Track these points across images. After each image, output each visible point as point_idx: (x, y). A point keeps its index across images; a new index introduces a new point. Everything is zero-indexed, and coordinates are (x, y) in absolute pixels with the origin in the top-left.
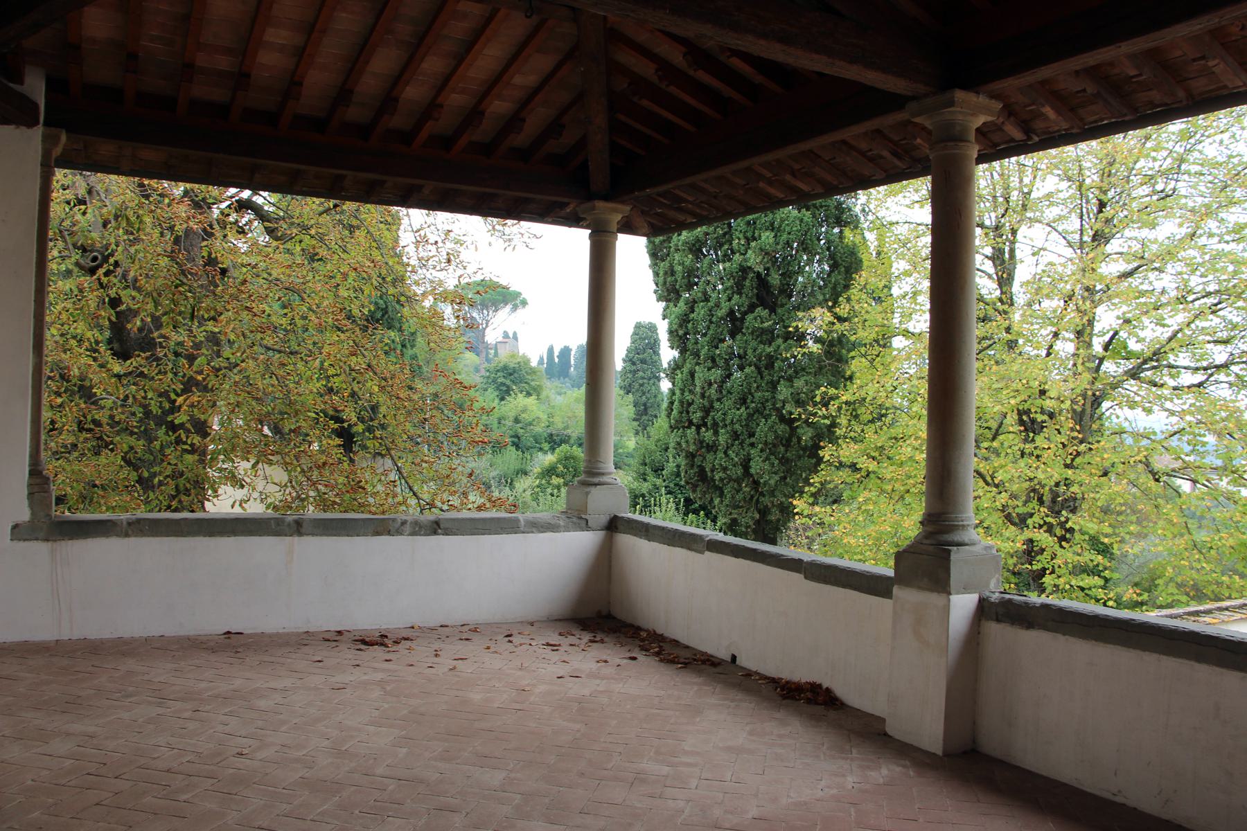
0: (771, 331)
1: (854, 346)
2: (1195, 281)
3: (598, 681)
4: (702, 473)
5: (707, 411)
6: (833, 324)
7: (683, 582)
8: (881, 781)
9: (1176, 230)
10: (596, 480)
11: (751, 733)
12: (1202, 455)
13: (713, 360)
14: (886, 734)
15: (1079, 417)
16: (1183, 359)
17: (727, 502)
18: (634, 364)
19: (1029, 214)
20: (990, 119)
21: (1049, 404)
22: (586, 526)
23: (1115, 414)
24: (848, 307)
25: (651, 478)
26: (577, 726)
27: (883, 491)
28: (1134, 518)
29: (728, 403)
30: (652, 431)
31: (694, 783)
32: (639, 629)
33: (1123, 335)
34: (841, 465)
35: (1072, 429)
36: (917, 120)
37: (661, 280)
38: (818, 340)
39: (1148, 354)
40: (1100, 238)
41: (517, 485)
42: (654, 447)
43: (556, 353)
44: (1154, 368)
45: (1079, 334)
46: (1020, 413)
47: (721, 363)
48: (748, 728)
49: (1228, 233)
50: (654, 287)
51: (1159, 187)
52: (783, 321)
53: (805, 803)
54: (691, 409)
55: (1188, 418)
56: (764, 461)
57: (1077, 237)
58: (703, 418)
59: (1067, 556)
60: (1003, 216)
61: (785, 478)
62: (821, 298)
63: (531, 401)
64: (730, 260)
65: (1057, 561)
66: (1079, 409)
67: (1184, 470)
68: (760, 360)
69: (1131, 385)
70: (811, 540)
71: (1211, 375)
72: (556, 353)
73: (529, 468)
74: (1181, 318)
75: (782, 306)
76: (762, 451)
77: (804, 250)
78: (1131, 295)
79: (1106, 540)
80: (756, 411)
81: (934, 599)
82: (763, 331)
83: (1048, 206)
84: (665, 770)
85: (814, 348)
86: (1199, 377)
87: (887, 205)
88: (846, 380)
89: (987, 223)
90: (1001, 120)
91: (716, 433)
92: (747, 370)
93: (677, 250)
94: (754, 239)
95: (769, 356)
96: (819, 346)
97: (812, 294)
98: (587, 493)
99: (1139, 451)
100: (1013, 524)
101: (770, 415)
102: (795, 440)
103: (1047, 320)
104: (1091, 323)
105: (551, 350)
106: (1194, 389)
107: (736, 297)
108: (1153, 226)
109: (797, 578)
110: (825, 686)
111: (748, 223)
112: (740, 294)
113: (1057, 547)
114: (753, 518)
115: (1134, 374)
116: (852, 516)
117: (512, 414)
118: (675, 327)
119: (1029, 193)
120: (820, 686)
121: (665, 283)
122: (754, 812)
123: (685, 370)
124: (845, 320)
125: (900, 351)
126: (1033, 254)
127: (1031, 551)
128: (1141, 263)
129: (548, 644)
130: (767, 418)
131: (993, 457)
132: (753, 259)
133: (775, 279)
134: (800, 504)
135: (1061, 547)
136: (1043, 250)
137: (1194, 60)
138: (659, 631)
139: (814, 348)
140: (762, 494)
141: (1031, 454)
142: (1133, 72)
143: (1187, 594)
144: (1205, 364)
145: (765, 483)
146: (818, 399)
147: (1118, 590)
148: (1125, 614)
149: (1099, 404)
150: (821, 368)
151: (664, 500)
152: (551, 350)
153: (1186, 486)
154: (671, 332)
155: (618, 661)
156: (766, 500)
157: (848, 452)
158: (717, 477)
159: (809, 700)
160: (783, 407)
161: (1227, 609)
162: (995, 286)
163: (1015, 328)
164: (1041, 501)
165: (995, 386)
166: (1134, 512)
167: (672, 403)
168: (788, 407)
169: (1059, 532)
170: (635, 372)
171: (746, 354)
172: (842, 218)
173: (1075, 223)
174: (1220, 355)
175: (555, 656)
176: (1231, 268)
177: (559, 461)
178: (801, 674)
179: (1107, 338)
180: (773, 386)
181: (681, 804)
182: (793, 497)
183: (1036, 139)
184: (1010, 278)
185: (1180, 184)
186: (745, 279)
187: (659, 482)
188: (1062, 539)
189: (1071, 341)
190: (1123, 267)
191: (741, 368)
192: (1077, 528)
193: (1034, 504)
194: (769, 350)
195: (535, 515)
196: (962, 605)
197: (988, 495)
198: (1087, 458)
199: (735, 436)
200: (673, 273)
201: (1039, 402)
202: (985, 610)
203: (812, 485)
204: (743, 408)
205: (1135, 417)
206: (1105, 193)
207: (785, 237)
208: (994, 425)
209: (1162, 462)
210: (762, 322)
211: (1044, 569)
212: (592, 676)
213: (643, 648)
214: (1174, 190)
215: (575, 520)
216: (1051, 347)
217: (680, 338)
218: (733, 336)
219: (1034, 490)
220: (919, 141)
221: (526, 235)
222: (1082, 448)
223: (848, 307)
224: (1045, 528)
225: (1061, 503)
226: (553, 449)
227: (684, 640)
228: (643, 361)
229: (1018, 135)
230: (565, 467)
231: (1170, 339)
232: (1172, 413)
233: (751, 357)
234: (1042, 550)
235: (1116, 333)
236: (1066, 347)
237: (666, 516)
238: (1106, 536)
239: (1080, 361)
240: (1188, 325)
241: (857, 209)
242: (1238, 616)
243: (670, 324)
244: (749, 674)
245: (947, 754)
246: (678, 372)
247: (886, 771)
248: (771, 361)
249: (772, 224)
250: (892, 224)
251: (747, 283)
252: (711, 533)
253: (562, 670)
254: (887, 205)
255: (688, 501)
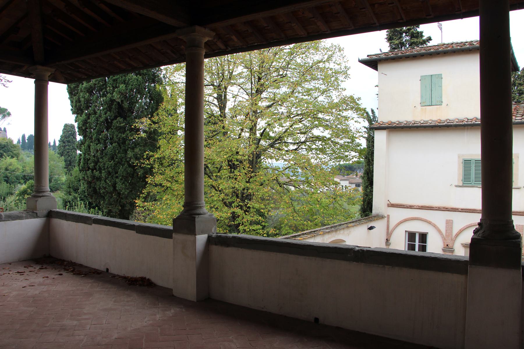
0: (124, 127)
1: (161, 134)
2: (293, 109)
3: (43, 287)
4: (95, 191)
5: (96, 163)
6: (151, 125)
7: (87, 239)
8: (171, 315)
9: (287, 90)
10: (41, 195)
11: (115, 302)
12: (297, 176)
13: (99, 140)
14: (173, 296)
15: (251, 163)
16: (290, 140)
17: (106, 202)
18: (64, 143)
19: (232, 81)
20: (210, 39)
21: (239, 157)
22: (36, 216)
23: (268, 162)
24: (157, 118)
25: (73, 194)
26: (32, 309)
27: (174, 195)
28: (272, 201)
29: (106, 159)
30: (73, 173)
31: (88, 327)
32: (64, 261)
33: (268, 130)
34: (156, 185)
35: (249, 167)
36: (180, 37)
37: (74, 104)
38: (145, 132)
39: (277, 138)
40: (259, 92)
41: (7, 200)
42: (74, 180)
43: (26, 138)
44: (279, 143)
45: (251, 129)
46: (229, 161)
47: (102, 141)
48: (113, 300)
49: (305, 92)
50: (71, 108)
51: (281, 73)
52: (129, 123)
53: (139, 329)
54: (89, 162)
55: (292, 162)
56: (122, 184)
57: (250, 91)
58: (94, 166)
59: (248, 218)
60: (221, 81)
61: (132, 191)
62: (146, 113)
63: (14, 160)
64: (106, 96)
65: (244, 220)
66: (251, 159)
67: (290, 183)
68: (119, 140)
69: (271, 150)
70: (145, 217)
71: (300, 146)
72: (26, 138)
73: (13, 192)
74: (288, 124)
75: (129, 117)
76: (121, 179)
77: (139, 93)
78: (270, 114)
79: (262, 211)
80: (118, 162)
81: (190, 237)
82: (121, 128)
83: (239, 78)
84: (75, 323)
85: (143, 135)
86: (295, 147)
87: (175, 75)
88: (157, 148)
89: (215, 84)
90: (216, 40)
91: (101, 172)
92: (114, 145)
93: (81, 91)
94: (117, 87)
95: (123, 138)
96: (145, 134)
97: (142, 112)
98: (36, 201)
99: (274, 175)
100: (226, 206)
101: (124, 164)
102: (135, 175)
103: (239, 124)
104: (255, 125)
105: (24, 137)
106: (293, 151)
107: (108, 112)
108: (278, 88)
109: (133, 232)
110: (147, 278)
111: (114, 80)
112: (110, 111)
113: (244, 214)
114: (118, 209)
115: (272, 146)
116: (161, 206)
117: (4, 167)
118: (81, 125)
119: (232, 73)
120: (145, 278)
121: (76, 106)
122: (116, 336)
123: (86, 145)
124: (156, 123)
125: (180, 137)
126: (233, 97)
127: (234, 216)
128: (274, 102)
129: (18, 272)
130: (123, 165)
131: (219, 179)
132: (116, 96)
133: (126, 105)
134: (138, 202)
135: (246, 214)
136: (237, 95)
137: (287, 23)
138: (74, 261)
139: (143, 135)
140: (122, 198)
141: (233, 178)
142: (266, 25)
143: (293, 230)
144: (297, 141)
145: (123, 193)
146: (145, 157)
147: (268, 230)
148: (270, 239)
149: (260, 157)
150: (146, 143)
151: (79, 203)
152: (24, 137)
153: (293, 188)
154: (79, 128)
155: (53, 276)
156: (123, 201)
157: (158, 179)
158: (101, 192)
159: (140, 285)
160: (130, 161)
161: (305, 234)
162: (218, 110)
163: (226, 126)
164: (237, 197)
165: (218, 150)
166: (273, 199)
167: (80, 160)
168: (132, 160)
169: (245, 208)
170: (65, 146)
171: (113, 138)
172: (155, 79)
173: (248, 86)
174: (303, 138)
175: (22, 278)
176: (306, 105)
177: (28, 188)
178: (138, 274)
179: (262, 131)
180: (126, 151)
181: (82, 337)
182: (136, 199)
183: (230, 49)
184: (225, 107)
185: (288, 72)
186: (112, 105)
187: (76, 195)
188: (245, 211)
189: (248, 132)
190: (268, 104)
191: (111, 144)
192: (251, 206)
193: (235, 198)
194: (124, 136)
195: (10, 212)
196: (201, 239)
197: (216, 195)
198: (255, 179)
199: (109, 173)
200: (80, 102)
201: (236, 157)
202: (210, 241)
203: (143, 193)
204: (112, 162)
205: (273, 162)
206: (261, 74)
207: (130, 87)
208: (219, 166)
209: (283, 179)
210: (120, 124)
211: (239, 224)
212: (40, 284)
213: (65, 269)
214: (286, 74)
215: (31, 213)
216: (240, 134)
217: (83, 131)
218: (107, 130)
219: (234, 192)
220: (182, 47)
221: (4, 80)
222: (253, 175)
223: (157, 118)
224: (239, 207)
225: (245, 196)
226: (25, 182)
227: (85, 264)
228: (69, 142)
229: (222, 47)
230: (31, 190)
231: (285, 132)
232: (285, 160)
233: (115, 139)
234: (239, 216)
235: (265, 129)
236: (246, 135)
237: (81, 210)
238: (263, 209)
239: (251, 140)
240: (291, 126)
241: (162, 76)
242: (309, 236)
243: (79, 124)
244: (114, 276)
245: (197, 301)
246: (83, 146)
247: (172, 311)
248: (124, 140)
249: (125, 81)
250: (176, 83)
251: (113, 107)
252: (100, 217)
253: (25, 283)
254: (175, 75)
255: (90, 204)
